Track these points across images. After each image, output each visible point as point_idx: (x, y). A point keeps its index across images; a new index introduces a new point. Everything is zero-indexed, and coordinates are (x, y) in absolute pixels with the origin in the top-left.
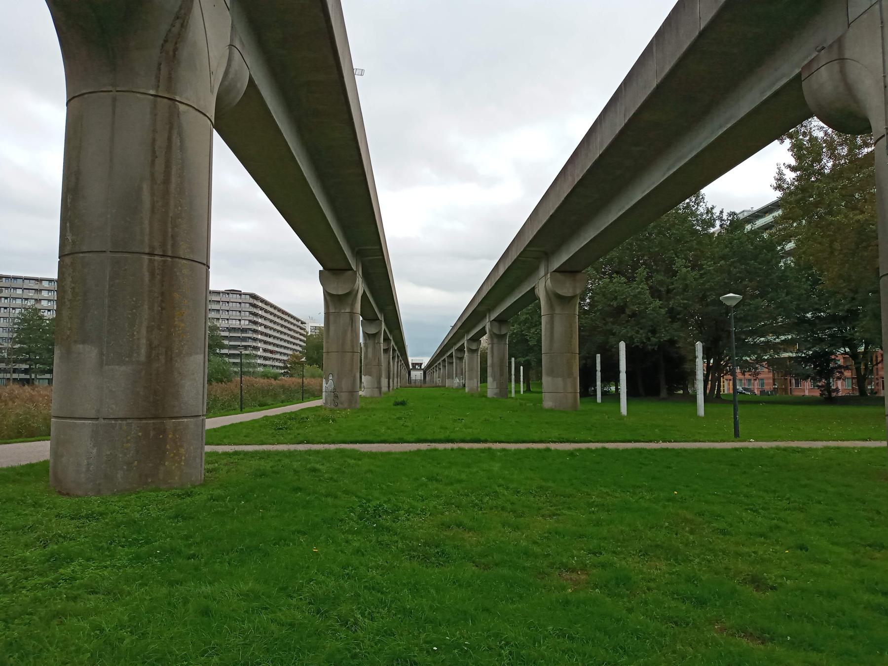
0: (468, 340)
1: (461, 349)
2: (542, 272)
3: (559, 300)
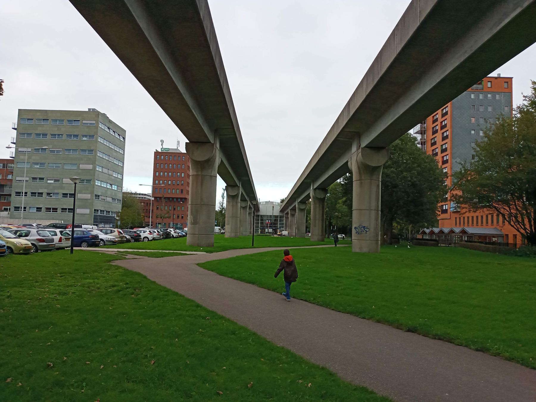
0: (315, 190)
1: (294, 209)
2: (354, 149)
3: (367, 170)
